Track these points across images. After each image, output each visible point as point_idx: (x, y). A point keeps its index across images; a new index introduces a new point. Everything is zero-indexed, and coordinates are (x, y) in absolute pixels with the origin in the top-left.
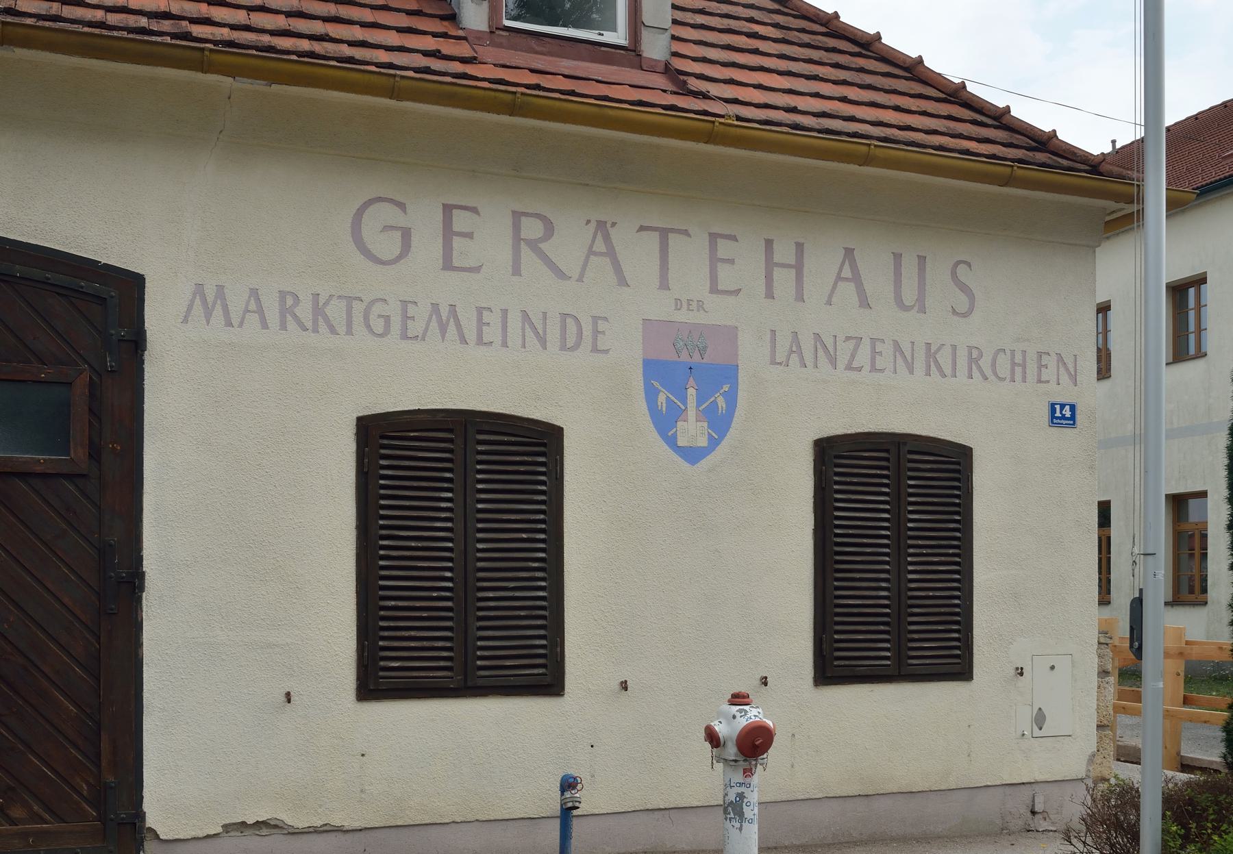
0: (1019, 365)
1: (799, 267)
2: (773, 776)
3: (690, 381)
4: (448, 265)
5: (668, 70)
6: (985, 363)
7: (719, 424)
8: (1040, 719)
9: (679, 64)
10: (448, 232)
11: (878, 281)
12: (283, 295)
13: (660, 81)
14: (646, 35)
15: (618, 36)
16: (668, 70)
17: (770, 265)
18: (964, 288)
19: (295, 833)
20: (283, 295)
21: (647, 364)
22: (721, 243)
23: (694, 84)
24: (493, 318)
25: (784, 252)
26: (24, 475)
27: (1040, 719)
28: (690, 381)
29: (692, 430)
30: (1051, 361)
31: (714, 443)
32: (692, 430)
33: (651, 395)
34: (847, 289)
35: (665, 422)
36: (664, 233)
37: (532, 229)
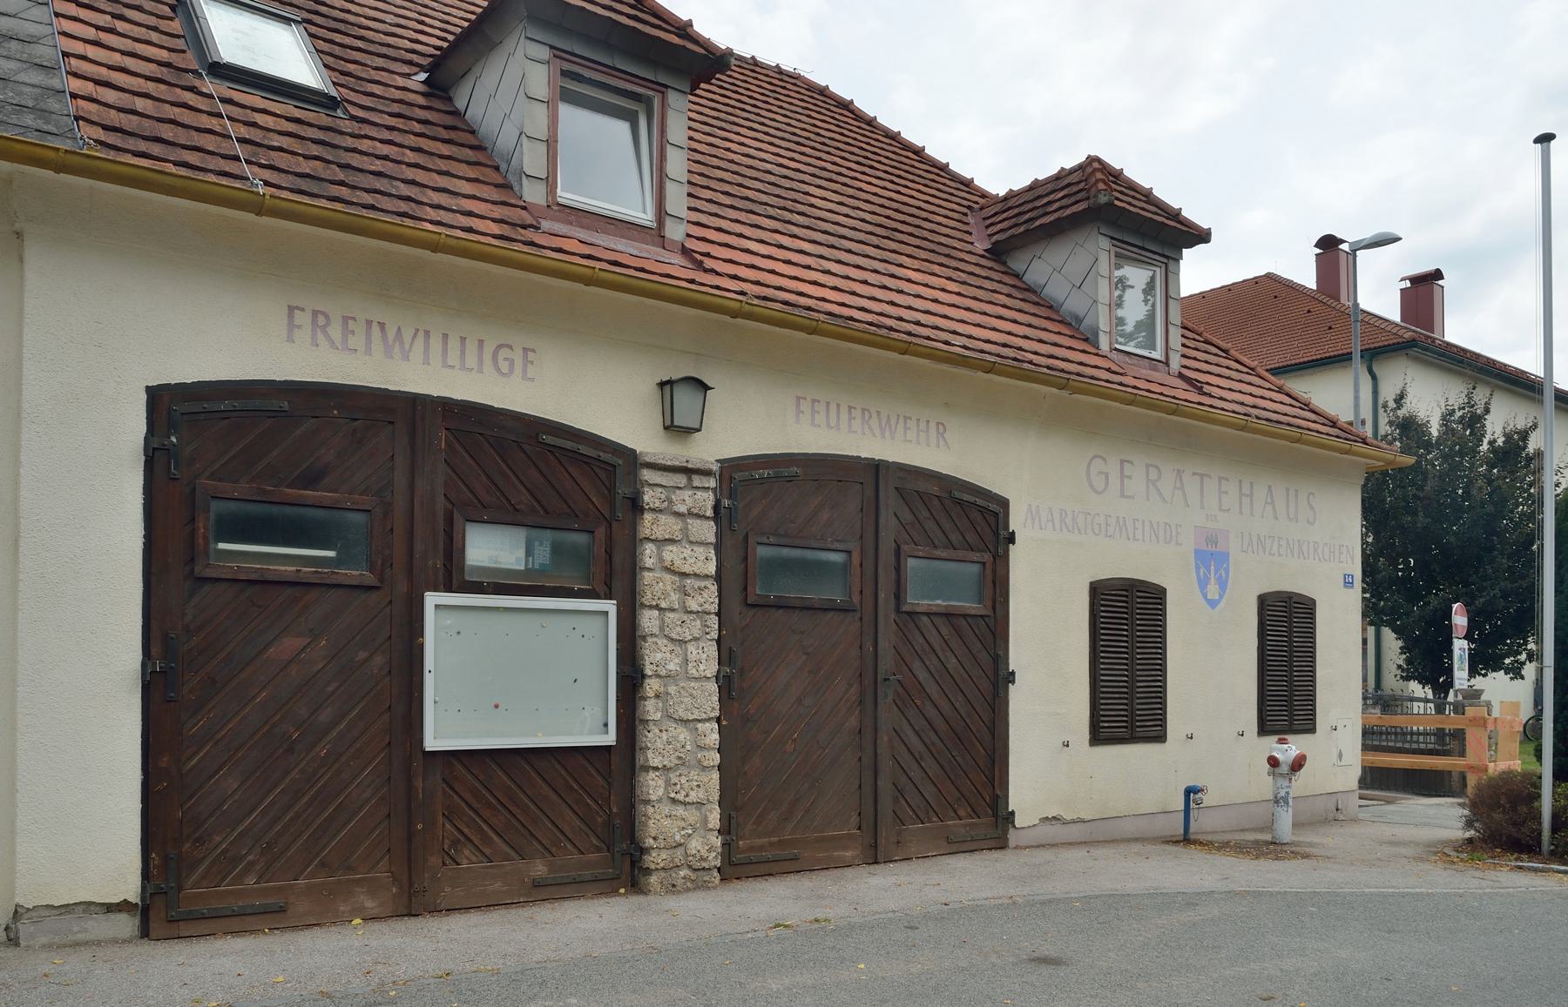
0: (690, 479)
1: (1251, 496)
2: (1301, 784)
3: (1211, 560)
4: (1123, 496)
5: (686, 252)
6: (1069, 521)
7: (1223, 585)
8: (1340, 756)
9: (692, 244)
10: (1123, 476)
11: (1137, 483)
12: (1061, 510)
13: (678, 259)
14: (669, 223)
15: (1157, 354)
16: (686, 252)
17: (1241, 495)
18: (1312, 508)
19: (1066, 823)
20: (1061, 510)
21: (1196, 552)
22: (1127, 466)
23: (709, 263)
24: (1139, 525)
25: (1292, 493)
26: (965, 616)
27: (1340, 756)
28: (1211, 560)
29: (1213, 590)
30: (1344, 550)
31: (1221, 597)
32: (1213, 590)
33: (1198, 568)
34: (1269, 508)
35: (1203, 584)
36: (1202, 476)
37: (1153, 474)
